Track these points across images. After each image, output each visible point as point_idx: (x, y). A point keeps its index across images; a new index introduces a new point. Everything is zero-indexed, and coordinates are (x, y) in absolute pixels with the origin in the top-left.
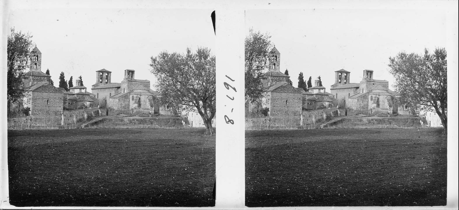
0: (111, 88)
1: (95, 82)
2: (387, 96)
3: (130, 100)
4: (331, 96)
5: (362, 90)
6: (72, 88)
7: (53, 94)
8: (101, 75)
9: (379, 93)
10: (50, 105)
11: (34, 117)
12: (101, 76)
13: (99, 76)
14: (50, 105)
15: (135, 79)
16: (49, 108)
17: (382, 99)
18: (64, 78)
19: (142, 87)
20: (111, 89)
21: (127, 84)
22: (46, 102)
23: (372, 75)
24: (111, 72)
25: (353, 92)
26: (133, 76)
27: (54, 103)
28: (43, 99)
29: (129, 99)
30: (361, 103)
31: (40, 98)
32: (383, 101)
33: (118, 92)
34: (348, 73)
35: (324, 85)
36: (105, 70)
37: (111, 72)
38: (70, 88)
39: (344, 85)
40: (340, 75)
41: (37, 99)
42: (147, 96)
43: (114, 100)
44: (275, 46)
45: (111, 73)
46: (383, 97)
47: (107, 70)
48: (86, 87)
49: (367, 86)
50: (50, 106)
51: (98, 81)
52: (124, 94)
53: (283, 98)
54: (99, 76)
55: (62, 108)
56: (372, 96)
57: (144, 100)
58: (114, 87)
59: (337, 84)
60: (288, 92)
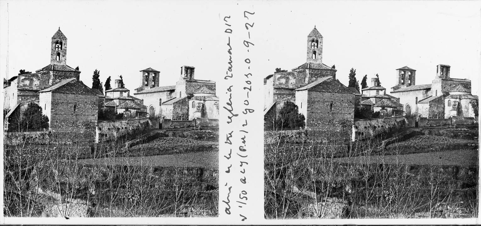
0: (161, 91)
1: (139, 84)
2: (471, 100)
3: (445, 105)
4: (394, 100)
5: (435, 92)
6: (109, 90)
7: (83, 96)
8: (402, 74)
9: (460, 95)
10: (78, 113)
11: (311, 130)
12: (403, 76)
13: (400, 75)
14: (78, 113)
15: (195, 79)
16: (333, 117)
17: (464, 104)
18: (355, 76)
19: (460, 87)
20: (417, 92)
21: (441, 84)
22: (329, 107)
23: (449, 72)
24: (416, 71)
25: (166, 97)
26: (193, 75)
27: (340, 109)
28: (324, 102)
29: (188, 106)
30: (178, 111)
31: (63, 102)
32: (210, 109)
33: (427, 96)
34: (413, 71)
35: (383, 85)
36: (152, 69)
37: (416, 71)
38: (363, 89)
39: (408, 87)
40: (146, 76)
41: (59, 104)
42: (469, 100)
43: (423, 106)
44: (59, 28)
45: (416, 72)
46: (466, 102)
47: (154, 69)
48: (129, 90)
49: (186, 88)
50: (78, 115)
51: (143, 84)
52: (437, 97)
53: (326, 100)
54: (144, 77)
55: (96, 118)
56: (193, 102)
57: (466, 106)
58: (422, 89)
59: (398, 85)
60: (77, 93)
